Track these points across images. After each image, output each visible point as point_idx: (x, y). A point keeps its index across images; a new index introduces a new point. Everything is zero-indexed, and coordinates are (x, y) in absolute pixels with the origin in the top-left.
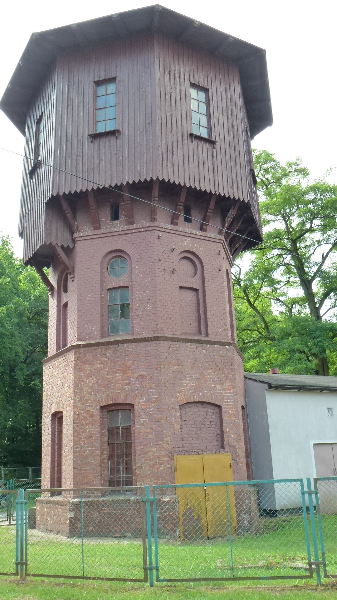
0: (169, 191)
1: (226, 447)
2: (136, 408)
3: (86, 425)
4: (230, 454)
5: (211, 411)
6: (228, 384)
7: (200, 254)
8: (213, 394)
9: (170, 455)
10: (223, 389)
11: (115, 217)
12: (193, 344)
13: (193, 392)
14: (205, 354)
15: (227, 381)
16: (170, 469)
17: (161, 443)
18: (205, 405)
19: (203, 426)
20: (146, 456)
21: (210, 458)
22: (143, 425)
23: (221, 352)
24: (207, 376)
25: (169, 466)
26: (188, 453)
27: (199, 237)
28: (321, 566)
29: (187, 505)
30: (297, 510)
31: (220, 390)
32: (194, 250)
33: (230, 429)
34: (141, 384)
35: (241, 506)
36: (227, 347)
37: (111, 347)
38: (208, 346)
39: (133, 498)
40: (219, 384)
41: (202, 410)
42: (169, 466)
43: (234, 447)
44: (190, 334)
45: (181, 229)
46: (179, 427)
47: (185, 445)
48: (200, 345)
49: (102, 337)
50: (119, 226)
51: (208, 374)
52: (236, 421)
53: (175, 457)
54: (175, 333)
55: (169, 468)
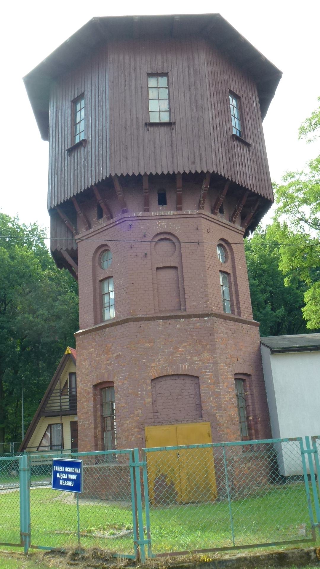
0: (132, 183)
1: (205, 417)
2: (115, 385)
3: (85, 402)
4: (209, 423)
5: (189, 382)
6: (207, 355)
7: (177, 233)
8: (189, 366)
9: (141, 426)
10: (200, 360)
11: (100, 216)
12: (165, 321)
13: (166, 366)
14: (179, 329)
15: (206, 352)
16: (141, 439)
17: (132, 415)
18: (182, 377)
19: (180, 397)
20: (123, 428)
21: (184, 428)
22: (120, 400)
23: (198, 324)
24: (181, 349)
25: (139, 436)
26: (160, 424)
27: (174, 217)
28: (28, 537)
29: (159, 471)
30: (300, 477)
31: (197, 361)
32: (170, 230)
33: (209, 398)
34: (118, 363)
35: (222, 473)
36: (206, 318)
37: (98, 332)
38: (183, 320)
39: (112, 465)
40: (196, 356)
41: (179, 382)
42: (139, 436)
43: (214, 415)
44: (172, 311)
45: (153, 213)
46: (150, 400)
47: (160, 417)
48: (173, 321)
49: (95, 324)
50: (103, 223)
51: (183, 347)
52: (216, 390)
53: (146, 428)
54: (148, 313)
55: (140, 438)
